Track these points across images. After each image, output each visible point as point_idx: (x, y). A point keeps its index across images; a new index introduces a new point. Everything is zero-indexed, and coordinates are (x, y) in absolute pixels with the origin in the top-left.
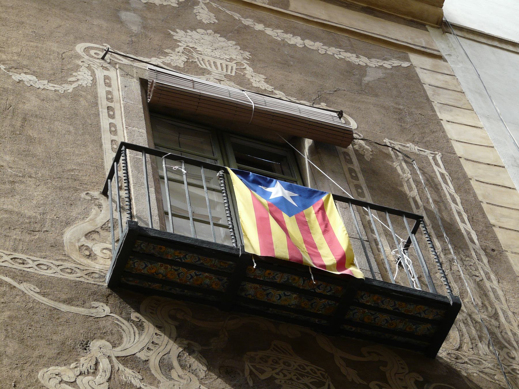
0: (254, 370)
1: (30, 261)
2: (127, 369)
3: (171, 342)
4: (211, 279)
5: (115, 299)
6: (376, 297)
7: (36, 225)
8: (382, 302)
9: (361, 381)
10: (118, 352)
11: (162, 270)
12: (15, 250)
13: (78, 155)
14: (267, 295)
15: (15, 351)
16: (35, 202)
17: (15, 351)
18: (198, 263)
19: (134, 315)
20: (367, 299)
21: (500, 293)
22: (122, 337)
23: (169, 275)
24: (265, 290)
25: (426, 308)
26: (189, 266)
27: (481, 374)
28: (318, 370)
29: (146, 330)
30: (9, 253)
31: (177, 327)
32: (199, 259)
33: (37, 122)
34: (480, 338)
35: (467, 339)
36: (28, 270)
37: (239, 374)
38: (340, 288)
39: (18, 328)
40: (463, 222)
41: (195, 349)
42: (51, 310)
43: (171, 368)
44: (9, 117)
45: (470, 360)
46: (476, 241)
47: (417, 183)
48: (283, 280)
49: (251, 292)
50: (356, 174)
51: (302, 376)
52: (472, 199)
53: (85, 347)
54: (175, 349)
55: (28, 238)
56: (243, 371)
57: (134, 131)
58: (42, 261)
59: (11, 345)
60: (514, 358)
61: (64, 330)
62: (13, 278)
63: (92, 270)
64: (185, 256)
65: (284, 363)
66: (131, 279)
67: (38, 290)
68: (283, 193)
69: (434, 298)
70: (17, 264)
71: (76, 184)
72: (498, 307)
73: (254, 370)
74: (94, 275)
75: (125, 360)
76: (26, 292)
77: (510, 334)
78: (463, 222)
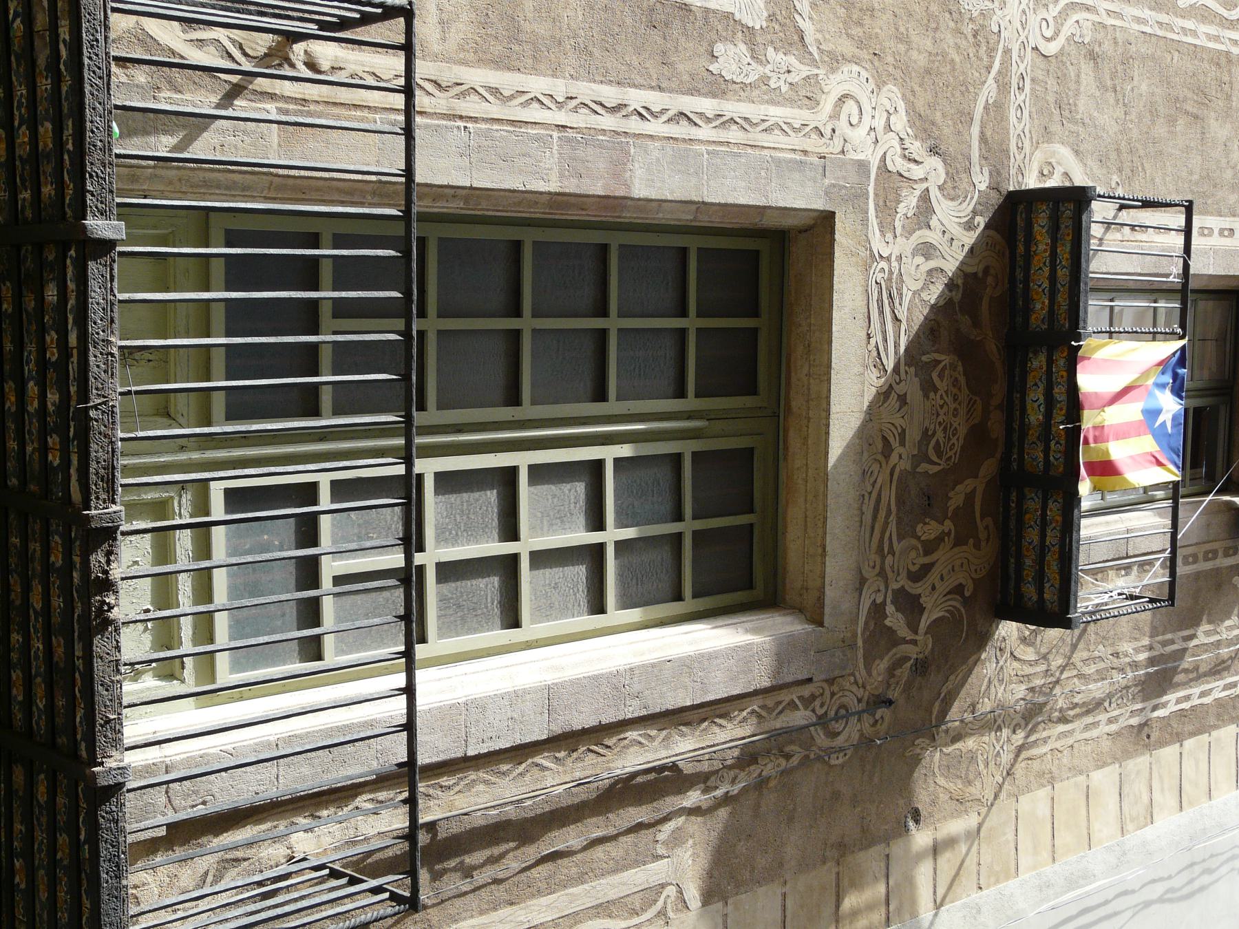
0: (941, 366)
1: (1023, 97)
2: (916, 199)
3: (957, 264)
4: (1042, 309)
5: (996, 200)
6: (1059, 519)
7: (1067, 111)
8: (1055, 528)
9: (951, 509)
10: (935, 193)
11: (1041, 247)
12: (1033, 80)
13: (1164, 179)
14: (1036, 384)
15: (915, 62)
16: (1096, 114)
17: (915, 62)
18: (1059, 286)
19: (981, 221)
20: (1054, 509)
21: (1094, 733)
22: (952, 199)
23: (1036, 258)
24: (1040, 380)
25: (1057, 586)
26: (1053, 278)
27: (986, 680)
28: (955, 454)
29: (965, 233)
30: (1029, 71)
31: (975, 274)
32: (1063, 286)
33: (1196, 133)
34: (1032, 690)
35: (1028, 670)
36: (1012, 93)
37: (933, 346)
38: (1061, 469)
39: (943, 70)
40: (1178, 702)
41: (954, 293)
42: (969, 114)
43: (927, 257)
44: (1195, 97)
45: (1002, 668)
46: (1156, 714)
47: (1218, 644)
48: (1057, 396)
49: (1036, 364)
50: (1210, 559)
51: (945, 429)
52: (1212, 720)
53: (934, 151)
54: (951, 266)
55: (1051, 98)
56: (937, 351)
57: (1209, 258)
58: (1026, 113)
59: (921, 57)
60: (1014, 732)
61: (948, 126)
62: (999, 72)
63: (1026, 174)
64: (1064, 267)
65: (955, 409)
66: (1024, 215)
67: (991, 101)
68: (1168, 411)
69: (1072, 593)
70: (1016, 80)
71: (1127, 171)
72: (1077, 725)
73: (941, 366)
74: (1020, 176)
75: (925, 197)
76: (986, 85)
77: (1045, 734)
78: (1178, 702)
